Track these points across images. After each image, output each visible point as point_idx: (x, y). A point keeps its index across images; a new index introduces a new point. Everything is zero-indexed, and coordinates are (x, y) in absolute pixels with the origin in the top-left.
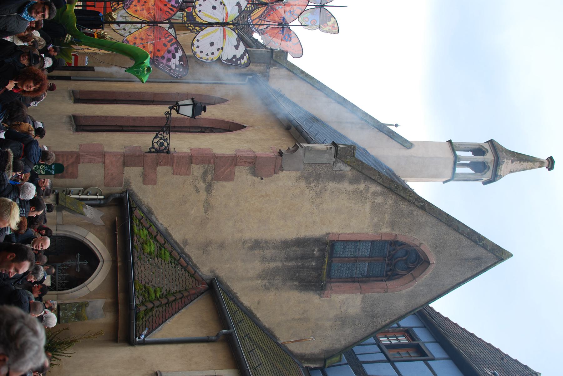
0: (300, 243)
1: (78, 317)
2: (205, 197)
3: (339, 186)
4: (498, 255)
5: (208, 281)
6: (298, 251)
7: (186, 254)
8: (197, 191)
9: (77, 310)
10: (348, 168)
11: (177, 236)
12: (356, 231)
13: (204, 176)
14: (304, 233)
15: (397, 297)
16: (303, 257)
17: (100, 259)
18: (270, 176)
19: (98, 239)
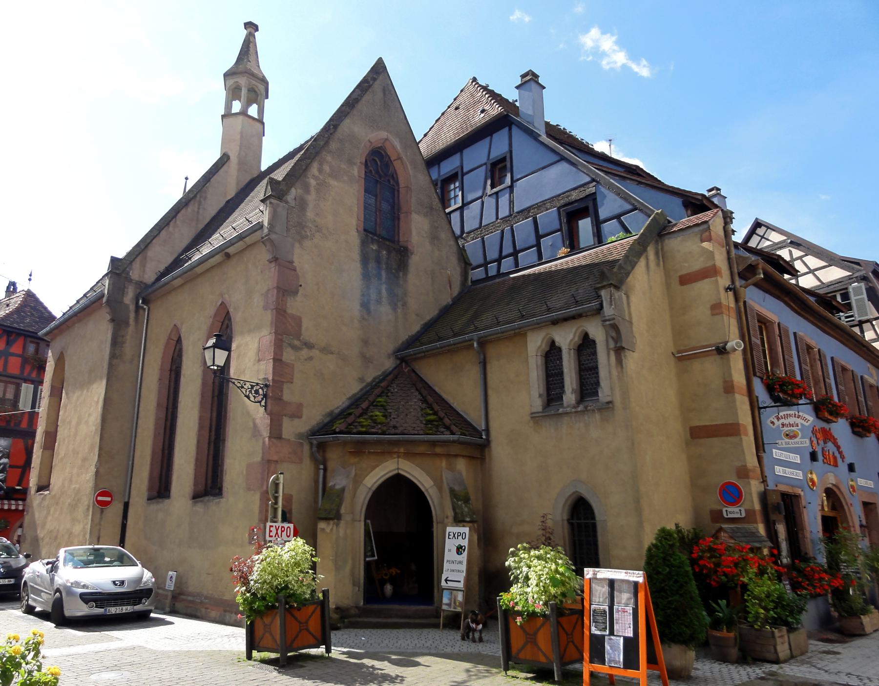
0: (365, 260)
1: (467, 500)
2: (318, 352)
3: (311, 205)
4: (379, 69)
5: (398, 362)
6: (372, 265)
7: (373, 381)
8: (311, 358)
9: (461, 500)
10: (293, 191)
11: (355, 388)
12: (355, 202)
13: (295, 348)
14: (356, 254)
15: (415, 182)
16: (378, 261)
17: (396, 472)
18: (298, 277)
19: (371, 474)
